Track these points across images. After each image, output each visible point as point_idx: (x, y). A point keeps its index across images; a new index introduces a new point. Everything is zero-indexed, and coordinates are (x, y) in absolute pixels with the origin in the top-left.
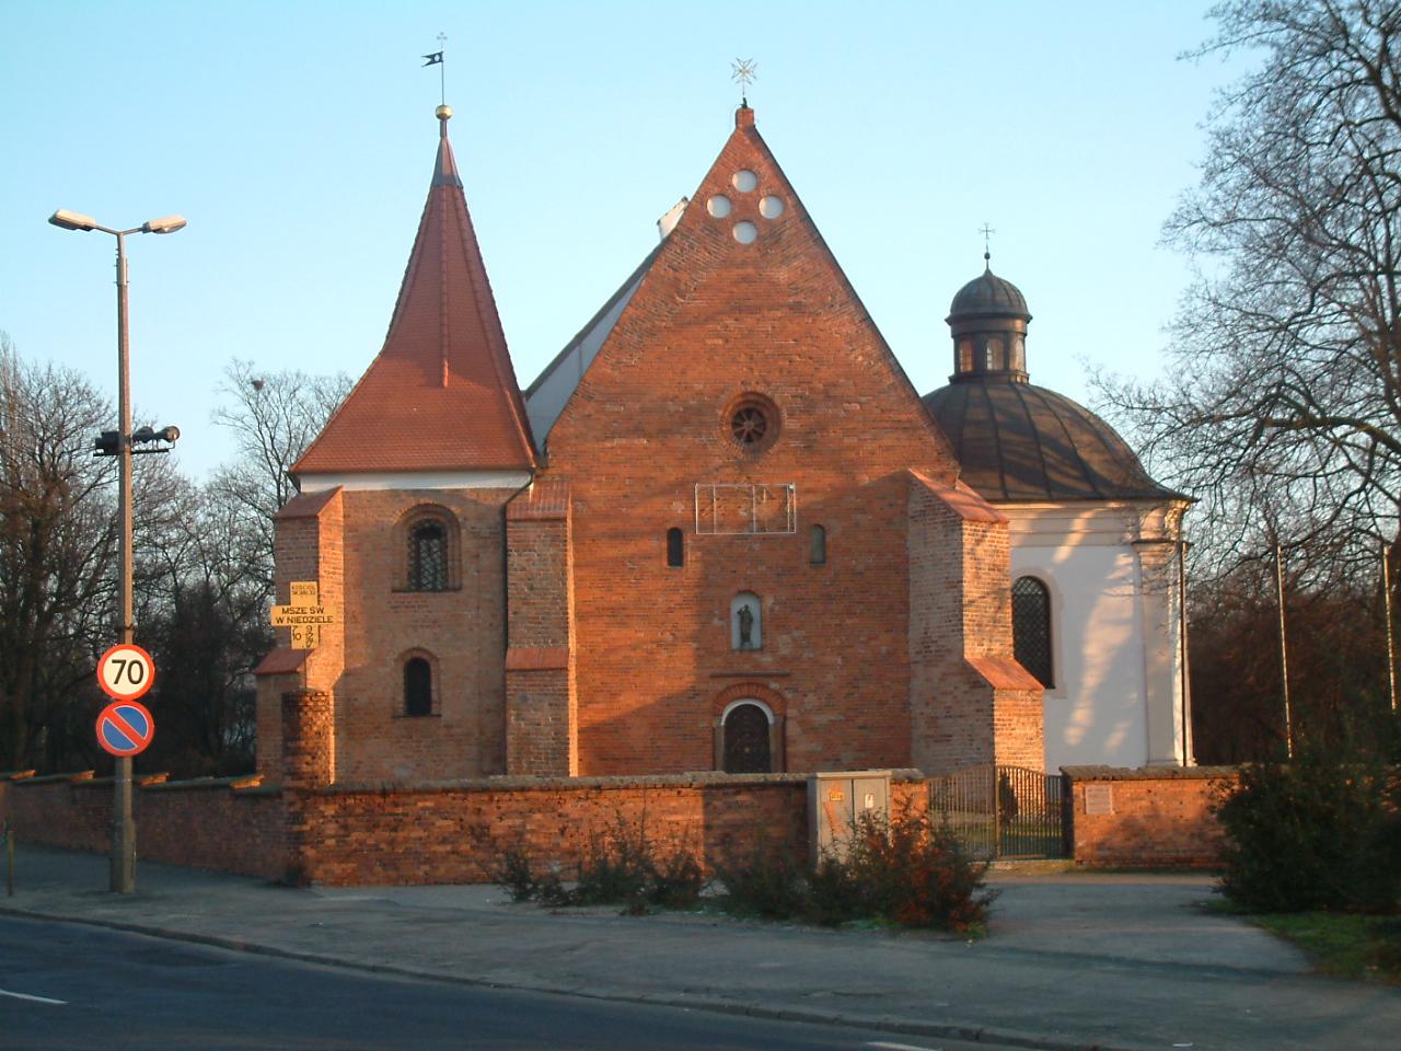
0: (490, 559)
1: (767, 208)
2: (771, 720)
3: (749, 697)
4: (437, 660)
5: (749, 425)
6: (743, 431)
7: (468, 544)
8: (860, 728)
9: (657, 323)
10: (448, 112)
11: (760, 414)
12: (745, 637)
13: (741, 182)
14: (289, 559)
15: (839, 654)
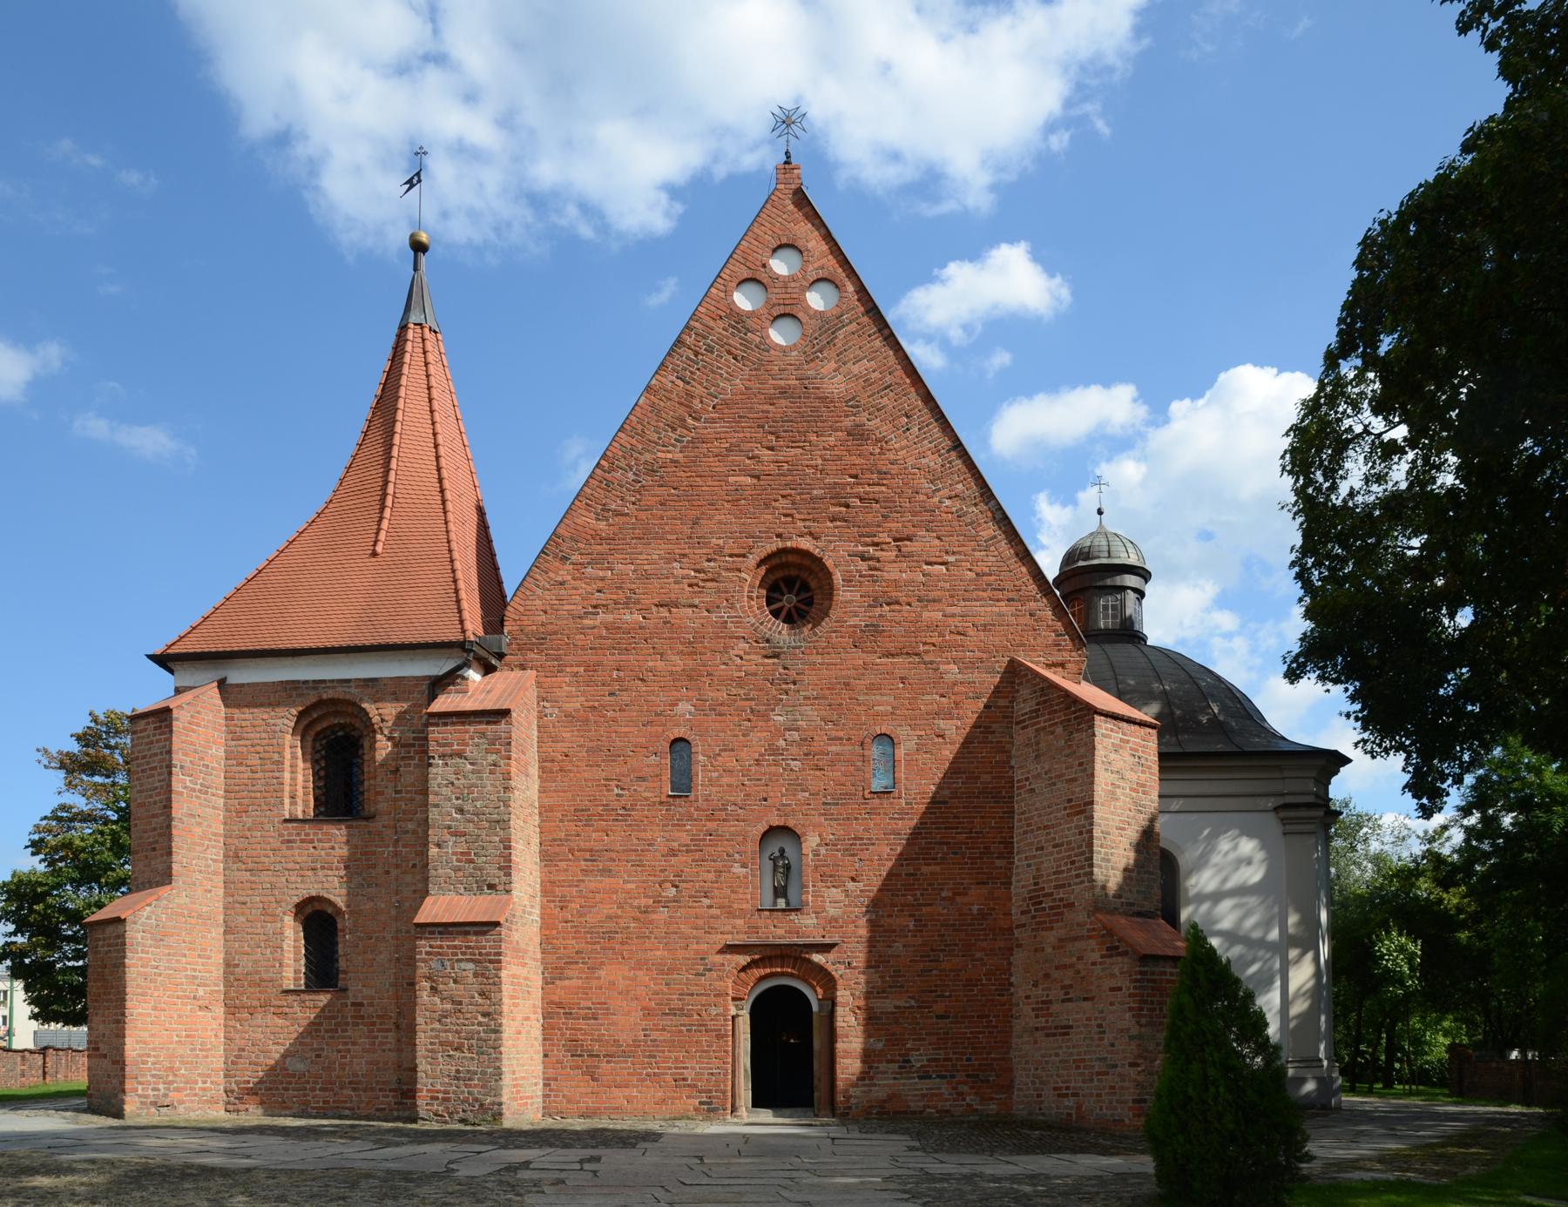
5: (789, 600)
10: (424, 237)
11: (805, 587)
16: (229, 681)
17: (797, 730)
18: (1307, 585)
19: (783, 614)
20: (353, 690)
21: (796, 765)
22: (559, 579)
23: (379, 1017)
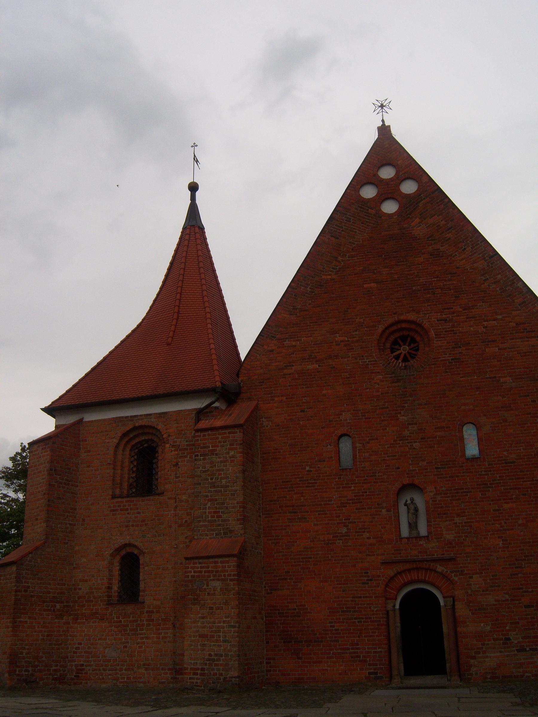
1: (409, 187)
2: (442, 603)
3: (419, 581)
5: (404, 349)
8: (526, 607)
9: (323, 277)
11: (413, 341)
12: (413, 526)
13: (387, 173)
15: (500, 537)
17: (416, 424)
20: (153, 420)
21: (416, 445)
22: (270, 348)
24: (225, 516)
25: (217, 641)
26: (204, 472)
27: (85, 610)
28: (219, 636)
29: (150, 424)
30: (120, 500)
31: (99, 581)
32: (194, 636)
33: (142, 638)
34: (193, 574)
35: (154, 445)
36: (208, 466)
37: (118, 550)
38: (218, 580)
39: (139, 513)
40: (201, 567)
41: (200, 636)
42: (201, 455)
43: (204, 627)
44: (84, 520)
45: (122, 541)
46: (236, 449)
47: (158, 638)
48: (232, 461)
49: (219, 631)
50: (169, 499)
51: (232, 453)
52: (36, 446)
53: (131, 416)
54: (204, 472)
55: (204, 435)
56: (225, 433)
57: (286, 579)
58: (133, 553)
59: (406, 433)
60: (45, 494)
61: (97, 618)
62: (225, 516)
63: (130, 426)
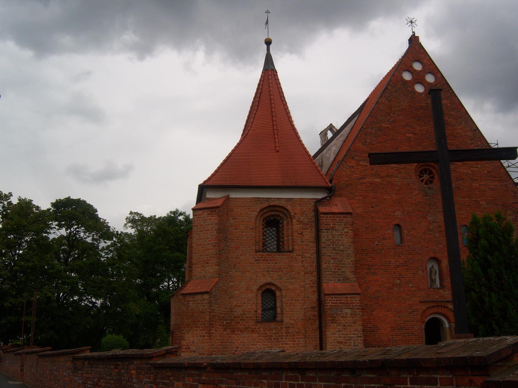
0: (309, 234)
1: (430, 78)
3: (431, 314)
4: (281, 290)
5: (426, 177)
6: (423, 180)
7: (297, 227)
14: (200, 231)
16: (230, 197)
17: (436, 222)
18: (181, 214)
19: (424, 181)
20: (283, 202)
21: (437, 235)
22: (351, 165)
23: (297, 332)
24: (343, 269)
25: (349, 345)
26: (328, 240)
27: (240, 325)
28: (351, 343)
29: (281, 205)
30: (262, 253)
31: (249, 307)
32: (334, 343)
33: (283, 344)
34: (331, 304)
35: (278, 218)
36: (330, 237)
37: (261, 287)
38: (349, 308)
39: (276, 263)
40: (336, 300)
41: (338, 342)
42: (325, 230)
43: (340, 337)
44: (235, 265)
45: (264, 281)
46: (348, 227)
47: (294, 344)
48: (346, 235)
49: (351, 340)
50: (297, 255)
51: (346, 230)
52: (200, 212)
53: (267, 198)
54: (328, 240)
55: (327, 217)
56: (341, 217)
57: (365, 309)
58: (271, 290)
59: (431, 227)
60: (214, 246)
61: (249, 331)
62: (343, 269)
63: (266, 204)
